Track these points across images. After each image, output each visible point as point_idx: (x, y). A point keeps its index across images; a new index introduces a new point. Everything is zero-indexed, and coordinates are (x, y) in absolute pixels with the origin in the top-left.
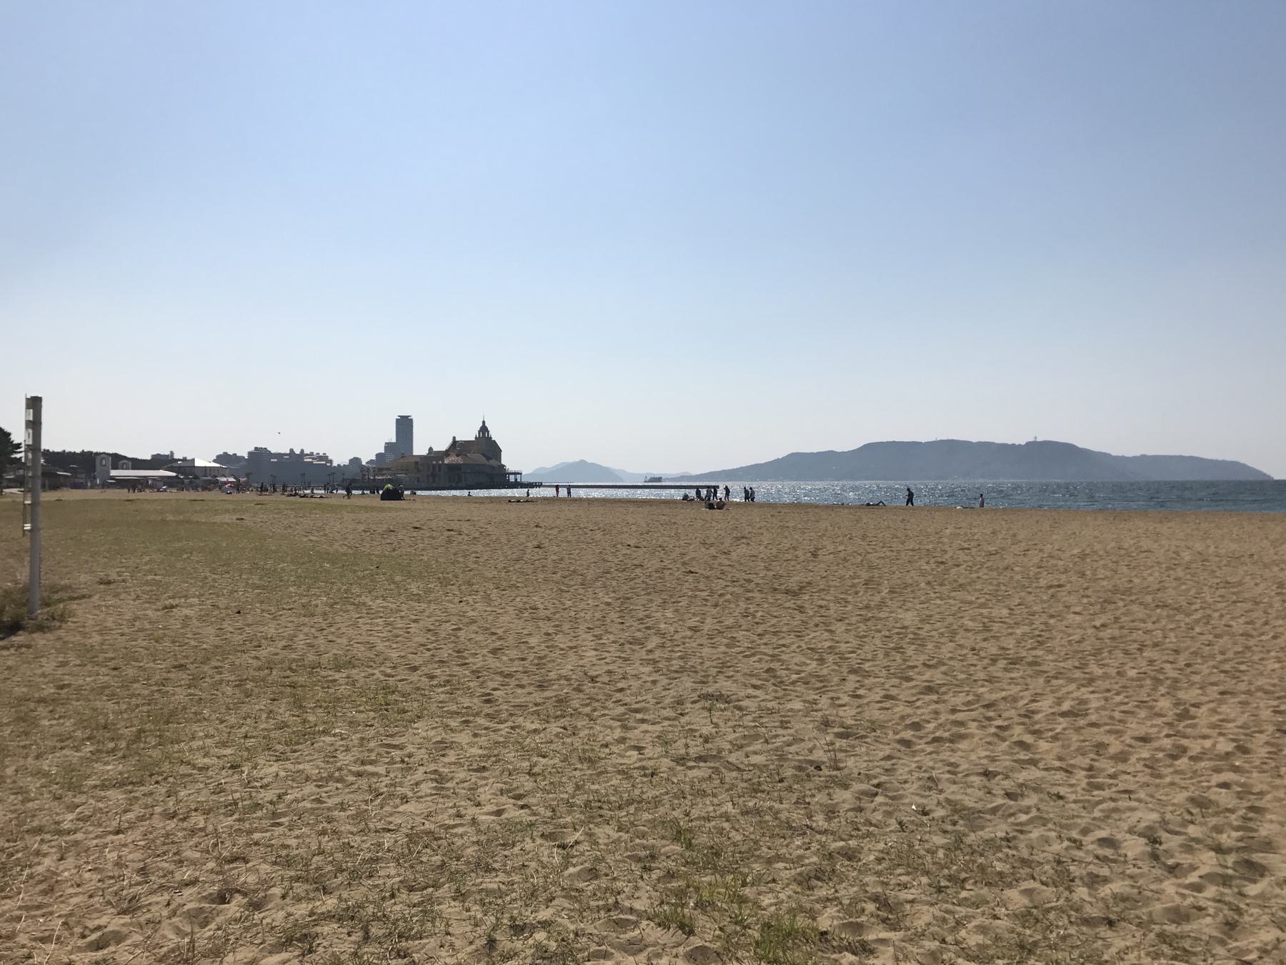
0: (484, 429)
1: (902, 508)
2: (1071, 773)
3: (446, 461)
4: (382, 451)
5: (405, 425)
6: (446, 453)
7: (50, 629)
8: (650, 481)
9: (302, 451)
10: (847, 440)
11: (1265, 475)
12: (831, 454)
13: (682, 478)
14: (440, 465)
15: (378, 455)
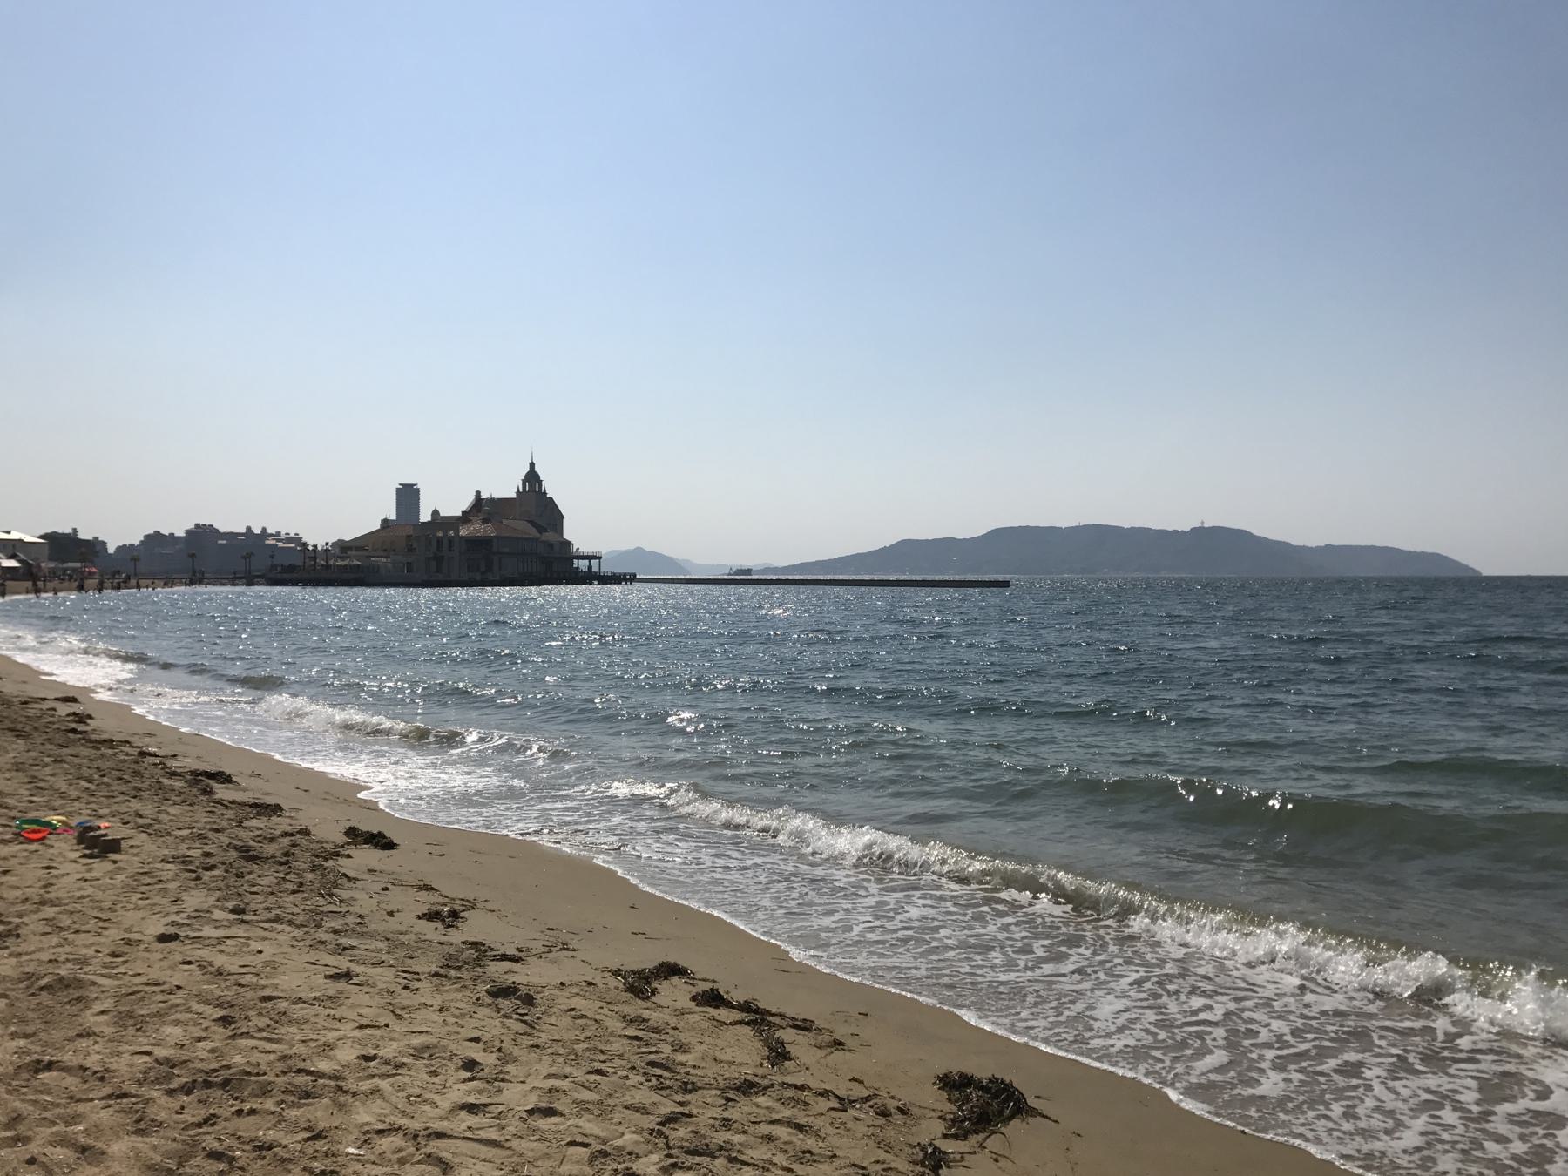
0: (532, 477)
6: (465, 517)
8: (736, 574)
9: (264, 530)
11: (1466, 568)
14: (451, 540)
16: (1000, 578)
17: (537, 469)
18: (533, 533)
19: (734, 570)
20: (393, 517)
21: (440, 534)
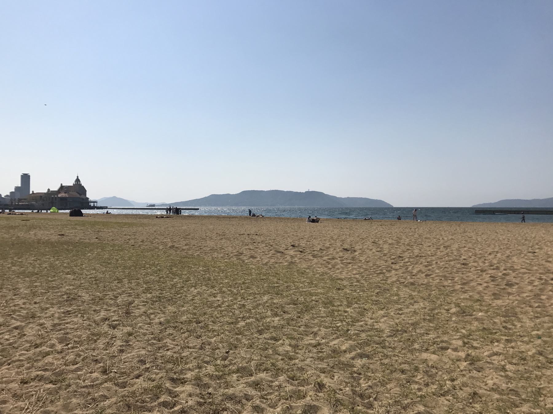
0: (78, 180)
1: (247, 217)
2: (549, 321)
3: (59, 196)
4: (14, 191)
5: (26, 178)
7: (467, 293)
8: (149, 206)
10: (235, 190)
12: (228, 195)
13: (163, 205)
15: (11, 193)
16: (196, 208)
17: (79, 178)
18: (78, 196)
19: (148, 205)
20: (20, 186)
21: (53, 196)
